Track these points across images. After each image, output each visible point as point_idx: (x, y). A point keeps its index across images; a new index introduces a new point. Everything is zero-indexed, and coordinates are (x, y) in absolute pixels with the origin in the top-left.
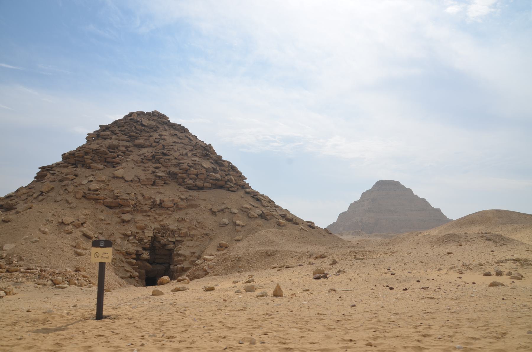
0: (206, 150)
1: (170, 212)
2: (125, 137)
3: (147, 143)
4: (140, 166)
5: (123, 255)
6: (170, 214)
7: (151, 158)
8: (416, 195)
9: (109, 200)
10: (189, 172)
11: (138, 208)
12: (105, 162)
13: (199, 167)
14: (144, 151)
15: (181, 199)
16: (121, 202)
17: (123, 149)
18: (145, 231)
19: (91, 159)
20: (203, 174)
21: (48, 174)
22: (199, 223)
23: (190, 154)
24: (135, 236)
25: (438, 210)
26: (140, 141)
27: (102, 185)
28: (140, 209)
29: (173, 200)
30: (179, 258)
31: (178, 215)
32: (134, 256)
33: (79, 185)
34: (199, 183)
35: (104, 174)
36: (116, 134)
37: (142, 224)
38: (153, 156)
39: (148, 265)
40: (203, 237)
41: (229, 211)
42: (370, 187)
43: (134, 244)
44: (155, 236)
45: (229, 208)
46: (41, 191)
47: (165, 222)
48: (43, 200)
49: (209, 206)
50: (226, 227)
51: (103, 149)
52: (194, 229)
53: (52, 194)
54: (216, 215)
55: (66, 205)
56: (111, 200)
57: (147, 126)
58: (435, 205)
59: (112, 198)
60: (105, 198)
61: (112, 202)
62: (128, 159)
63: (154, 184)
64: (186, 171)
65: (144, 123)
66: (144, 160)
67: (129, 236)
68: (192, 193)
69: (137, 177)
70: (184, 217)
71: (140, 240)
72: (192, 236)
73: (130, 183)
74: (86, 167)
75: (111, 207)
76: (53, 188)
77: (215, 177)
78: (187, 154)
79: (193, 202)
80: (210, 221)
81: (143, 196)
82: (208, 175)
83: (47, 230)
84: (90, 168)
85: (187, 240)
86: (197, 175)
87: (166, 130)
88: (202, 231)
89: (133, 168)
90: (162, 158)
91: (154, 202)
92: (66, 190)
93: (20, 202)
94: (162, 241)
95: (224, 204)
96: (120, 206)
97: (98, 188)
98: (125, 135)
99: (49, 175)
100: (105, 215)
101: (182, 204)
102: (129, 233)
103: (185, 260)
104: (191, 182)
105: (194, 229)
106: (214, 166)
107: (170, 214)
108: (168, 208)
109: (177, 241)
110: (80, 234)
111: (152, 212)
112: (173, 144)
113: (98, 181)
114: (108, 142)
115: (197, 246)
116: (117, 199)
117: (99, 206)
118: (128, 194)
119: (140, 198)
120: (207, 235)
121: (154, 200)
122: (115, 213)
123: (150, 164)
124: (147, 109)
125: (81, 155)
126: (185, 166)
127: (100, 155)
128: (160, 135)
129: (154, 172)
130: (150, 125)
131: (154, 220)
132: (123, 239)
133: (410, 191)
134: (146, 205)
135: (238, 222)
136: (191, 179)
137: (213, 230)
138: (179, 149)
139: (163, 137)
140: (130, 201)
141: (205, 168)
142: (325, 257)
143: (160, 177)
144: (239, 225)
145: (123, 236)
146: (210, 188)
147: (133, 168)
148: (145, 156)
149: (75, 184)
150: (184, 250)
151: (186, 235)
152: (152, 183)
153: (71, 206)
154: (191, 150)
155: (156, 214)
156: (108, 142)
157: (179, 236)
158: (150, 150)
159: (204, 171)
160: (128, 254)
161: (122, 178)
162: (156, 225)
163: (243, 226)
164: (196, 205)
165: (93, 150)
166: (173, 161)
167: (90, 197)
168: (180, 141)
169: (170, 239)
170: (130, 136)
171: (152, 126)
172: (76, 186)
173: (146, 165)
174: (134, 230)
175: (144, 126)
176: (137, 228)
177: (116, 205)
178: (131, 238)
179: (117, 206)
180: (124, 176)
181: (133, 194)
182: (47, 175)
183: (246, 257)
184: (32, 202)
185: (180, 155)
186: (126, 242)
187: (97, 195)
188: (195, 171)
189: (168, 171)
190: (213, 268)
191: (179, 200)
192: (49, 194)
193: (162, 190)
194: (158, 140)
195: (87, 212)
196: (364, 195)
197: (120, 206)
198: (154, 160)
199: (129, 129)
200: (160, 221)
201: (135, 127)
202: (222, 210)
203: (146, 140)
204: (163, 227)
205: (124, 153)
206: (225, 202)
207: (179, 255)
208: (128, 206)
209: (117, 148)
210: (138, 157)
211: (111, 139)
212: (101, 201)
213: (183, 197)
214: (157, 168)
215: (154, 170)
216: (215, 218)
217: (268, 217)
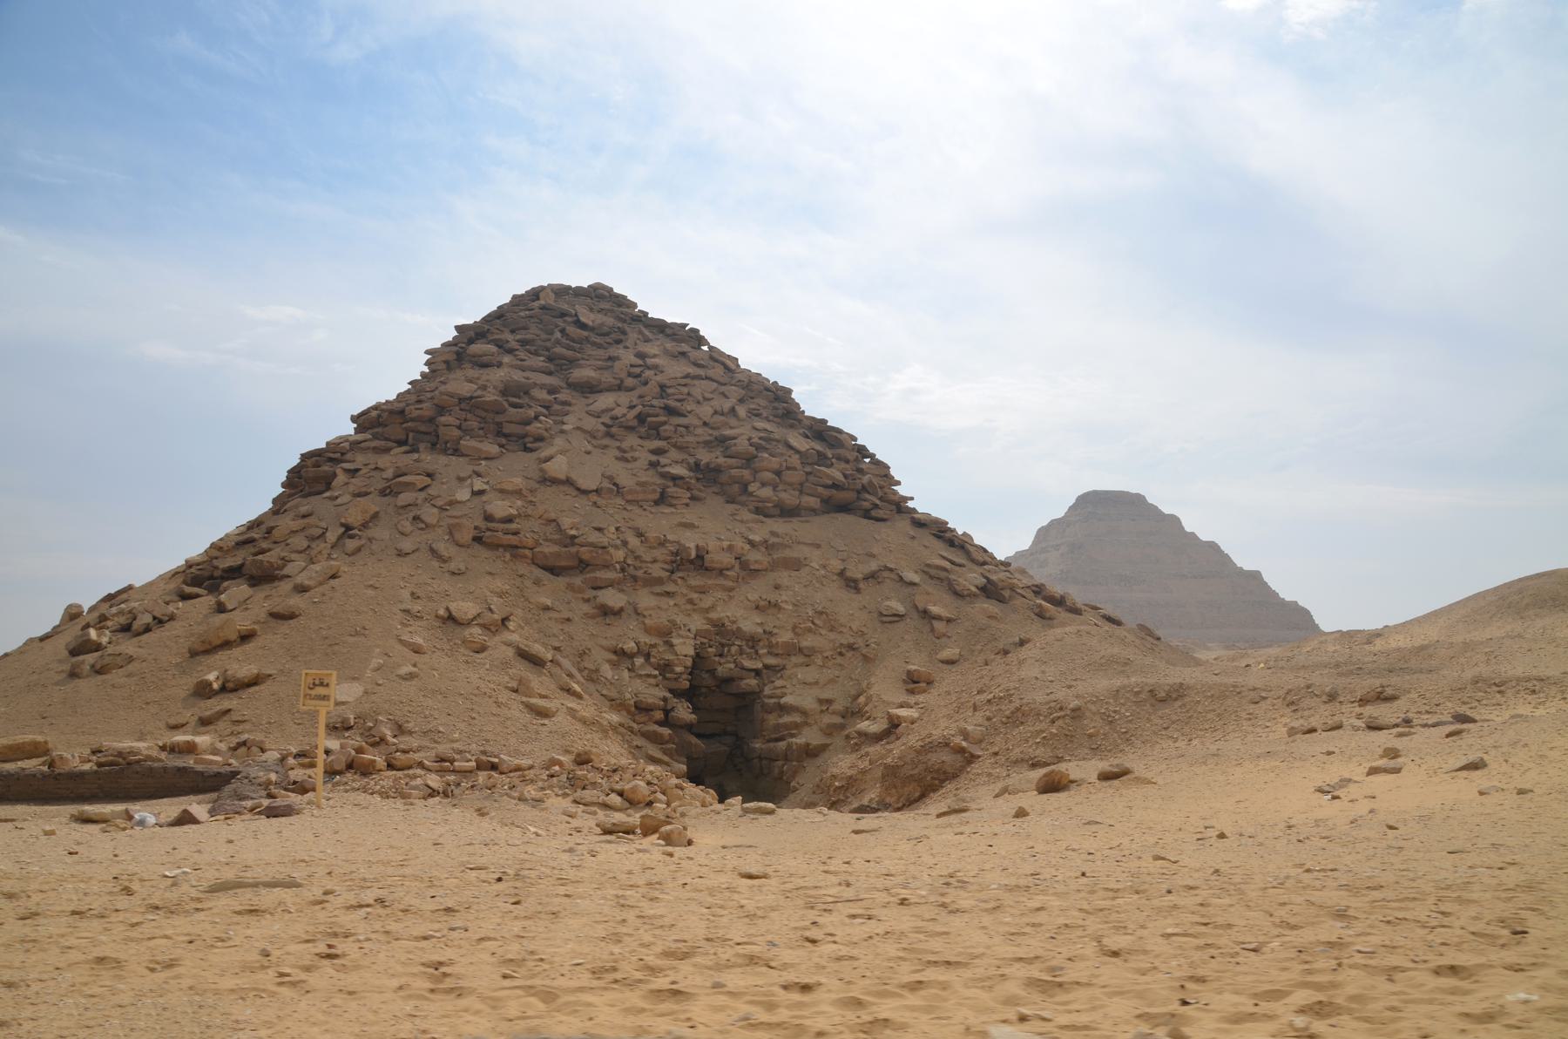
0: (777, 399)
1: (730, 584)
2: (539, 362)
3: (607, 378)
4: (606, 447)
5: (629, 712)
6: (731, 589)
7: (635, 423)
8: (1193, 534)
9: (548, 549)
10: (757, 464)
11: (631, 570)
12: (499, 434)
13: (781, 449)
14: (604, 401)
15: (752, 543)
16: (585, 553)
17: (542, 395)
18: (675, 641)
19: (459, 427)
20: (795, 469)
21: (339, 471)
22: (821, 613)
23: (742, 411)
24: (648, 656)
25: (1256, 576)
26: (584, 373)
27: (519, 503)
28: (640, 573)
29: (730, 548)
30: (786, 719)
31: (756, 590)
32: (659, 715)
33: (451, 503)
34: (789, 498)
35: (514, 470)
36: (510, 351)
37: (661, 619)
38: (641, 418)
39: (694, 740)
40: (841, 654)
41: (893, 576)
42: (1060, 513)
43: (652, 681)
44: (697, 655)
45: (891, 570)
46: (342, 525)
47: (723, 613)
48: (359, 550)
49: (836, 565)
50: (901, 625)
51: (491, 396)
52: (810, 630)
53: (381, 532)
54: (858, 590)
55: (436, 564)
56: (556, 548)
57: (592, 329)
58: (1244, 561)
59: (555, 542)
60: (538, 544)
61: (558, 555)
62: (565, 427)
63: (662, 499)
64: (749, 460)
65: (583, 319)
66: (612, 429)
67: (631, 656)
68: (779, 526)
69: (610, 478)
70: (773, 597)
71: (665, 668)
72: (808, 654)
73: (594, 497)
74: (444, 452)
75: (553, 571)
76: (375, 516)
77: (828, 476)
78: (733, 410)
79: (788, 553)
80: (851, 610)
81: (640, 535)
82: (808, 474)
83: (419, 640)
84: (457, 452)
85: (796, 665)
86: (778, 473)
87: (647, 340)
88: (832, 636)
89: (588, 453)
90: (665, 423)
91: (677, 554)
92: (416, 518)
93: (293, 556)
94: (720, 669)
95: (873, 556)
96: (583, 565)
97: (514, 512)
98: (536, 354)
99: (341, 478)
100: (550, 591)
101: (755, 557)
102: (630, 646)
103: (806, 724)
104: (766, 492)
105: (810, 630)
106: (818, 447)
107: (731, 589)
108: (721, 572)
109: (766, 667)
110: (510, 652)
111: (675, 582)
112: (687, 381)
113: (502, 491)
114: (497, 376)
115: (832, 681)
116: (573, 544)
117: (523, 568)
118: (599, 530)
119: (634, 542)
120: (851, 647)
121: (636, 552)
122: (570, 587)
123: (631, 440)
124: (580, 279)
125: (427, 413)
126: (742, 445)
127: (484, 414)
128: (641, 356)
129: (653, 465)
130: (602, 324)
131: (689, 607)
132: (614, 665)
133: (1174, 521)
134: (655, 561)
135: (934, 609)
136: (763, 485)
137: (863, 634)
138: (708, 395)
139: (650, 361)
140: (612, 550)
141: (798, 452)
142: (1393, 698)
143: (675, 478)
144: (939, 618)
145: (614, 657)
146: (814, 511)
147: (588, 453)
148: (614, 418)
149: (439, 503)
150: (799, 690)
151: (792, 650)
152: (657, 496)
153: (453, 566)
154: (741, 401)
155: (691, 588)
156: (497, 376)
157: (770, 653)
158: (624, 398)
159: (795, 460)
160: (642, 708)
161: (569, 482)
162: (697, 623)
163: (949, 621)
164: (798, 560)
165: (461, 400)
166: (699, 431)
167: (491, 538)
168: (701, 372)
169: (748, 664)
170: (550, 359)
171: (606, 329)
172: (442, 509)
173: (625, 445)
174: (646, 639)
175: (583, 326)
176: (648, 630)
177: (571, 563)
178: (639, 661)
179: (571, 568)
180: (574, 476)
181: (613, 529)
182: (335, 475)
183: (1093, 708)
184: (329, 557)
185: (716, 412)
186: (626, 674)
187: (516, 533)
188: (775, 463)
189: (692, 461)
190: (981, 741)
191: (747, 547)
192: (370, 533)
193: (689, 516)
194: (637, 370)
195: (499, 584)
196: (1043, 534)
197: (583, 565)
198: (643, 430)
199: (544, 336)
200: (707, 610)
201: (563, 331)
202: (872, 576)
203: (600, 369)
204: (719, 627)
205: (547, 408)
206: (875, 551)
207: (784, 709)
208: (607, 566)
209: (526, 393)
210: (593, 421)
211: (500, 365)
212: (527, 552)
213: (757, 538)
214: (658, 452)
215: (654, 458)
216: (859, 597)
217: (1007, 593)
